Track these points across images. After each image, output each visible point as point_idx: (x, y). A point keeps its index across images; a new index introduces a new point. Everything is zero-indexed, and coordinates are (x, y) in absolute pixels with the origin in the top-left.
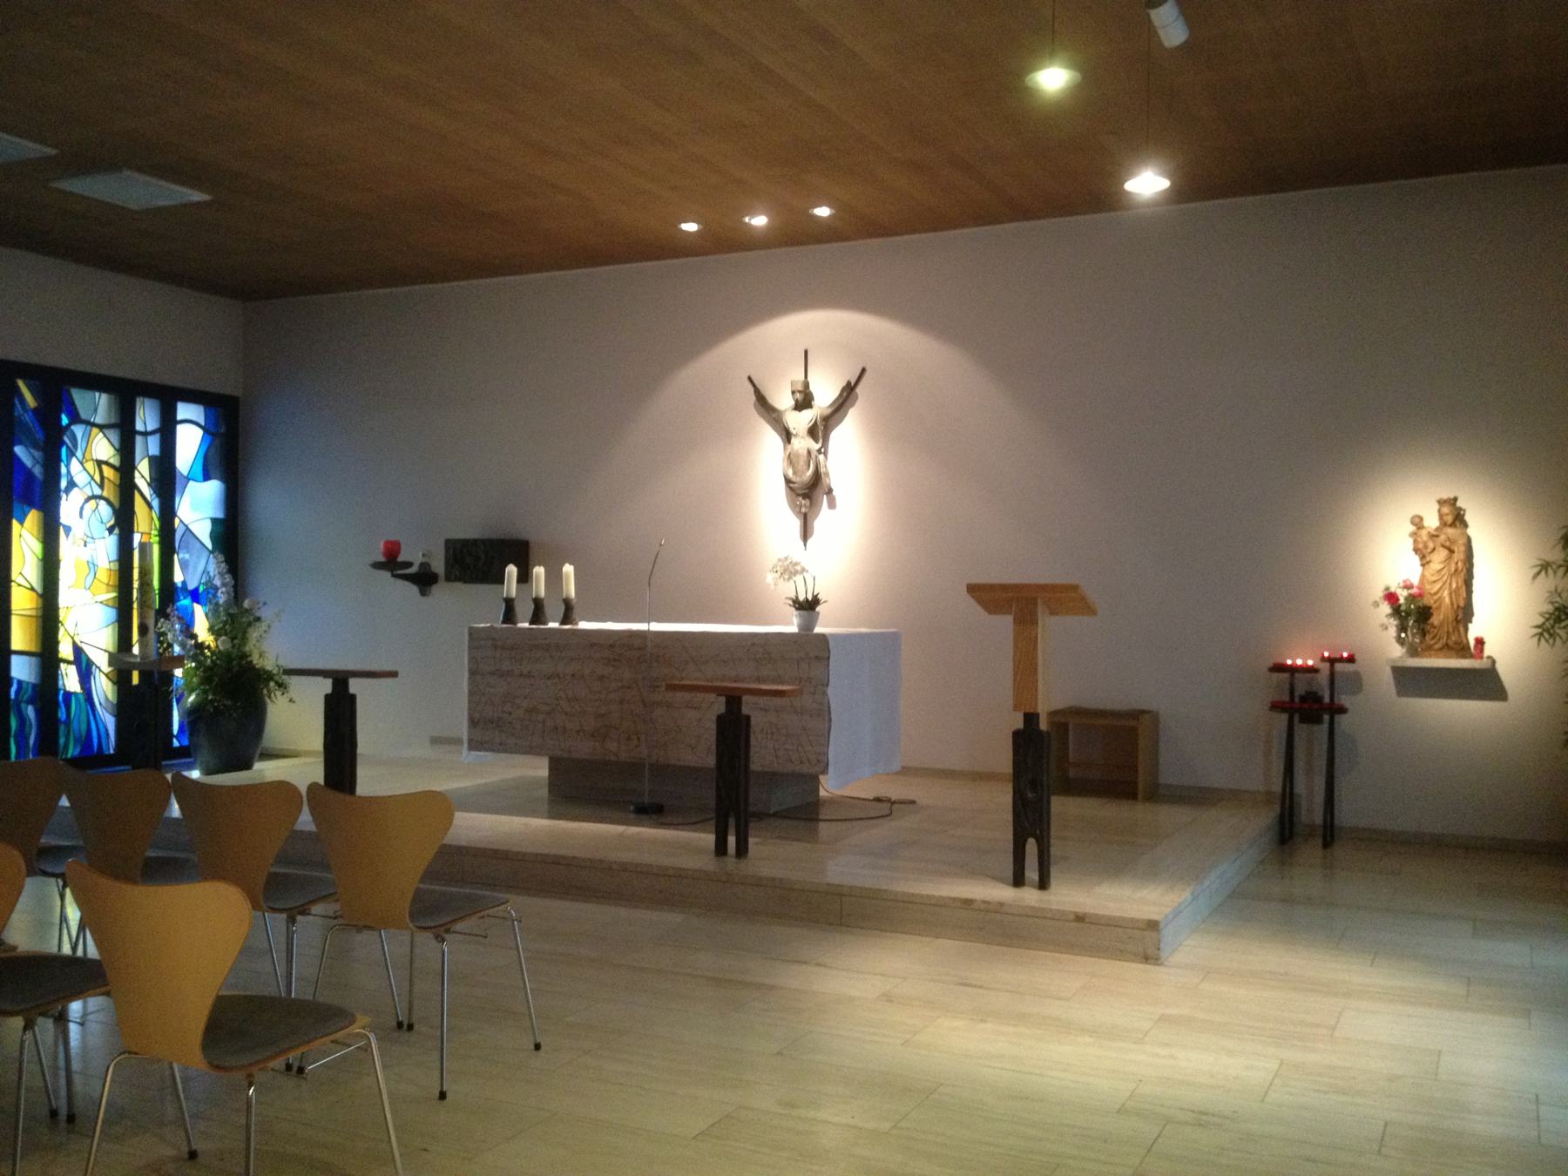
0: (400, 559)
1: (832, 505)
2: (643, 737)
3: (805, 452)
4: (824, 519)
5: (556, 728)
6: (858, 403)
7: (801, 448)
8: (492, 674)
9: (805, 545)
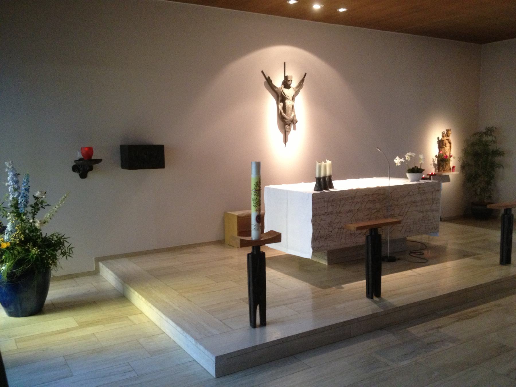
1: (295, 129)
3: (292, 107)
4: (292, 134)
5: (351, 234)
6: (304, 87)
7: (290, 104)
8: (324, 215)
9: (286, 145)
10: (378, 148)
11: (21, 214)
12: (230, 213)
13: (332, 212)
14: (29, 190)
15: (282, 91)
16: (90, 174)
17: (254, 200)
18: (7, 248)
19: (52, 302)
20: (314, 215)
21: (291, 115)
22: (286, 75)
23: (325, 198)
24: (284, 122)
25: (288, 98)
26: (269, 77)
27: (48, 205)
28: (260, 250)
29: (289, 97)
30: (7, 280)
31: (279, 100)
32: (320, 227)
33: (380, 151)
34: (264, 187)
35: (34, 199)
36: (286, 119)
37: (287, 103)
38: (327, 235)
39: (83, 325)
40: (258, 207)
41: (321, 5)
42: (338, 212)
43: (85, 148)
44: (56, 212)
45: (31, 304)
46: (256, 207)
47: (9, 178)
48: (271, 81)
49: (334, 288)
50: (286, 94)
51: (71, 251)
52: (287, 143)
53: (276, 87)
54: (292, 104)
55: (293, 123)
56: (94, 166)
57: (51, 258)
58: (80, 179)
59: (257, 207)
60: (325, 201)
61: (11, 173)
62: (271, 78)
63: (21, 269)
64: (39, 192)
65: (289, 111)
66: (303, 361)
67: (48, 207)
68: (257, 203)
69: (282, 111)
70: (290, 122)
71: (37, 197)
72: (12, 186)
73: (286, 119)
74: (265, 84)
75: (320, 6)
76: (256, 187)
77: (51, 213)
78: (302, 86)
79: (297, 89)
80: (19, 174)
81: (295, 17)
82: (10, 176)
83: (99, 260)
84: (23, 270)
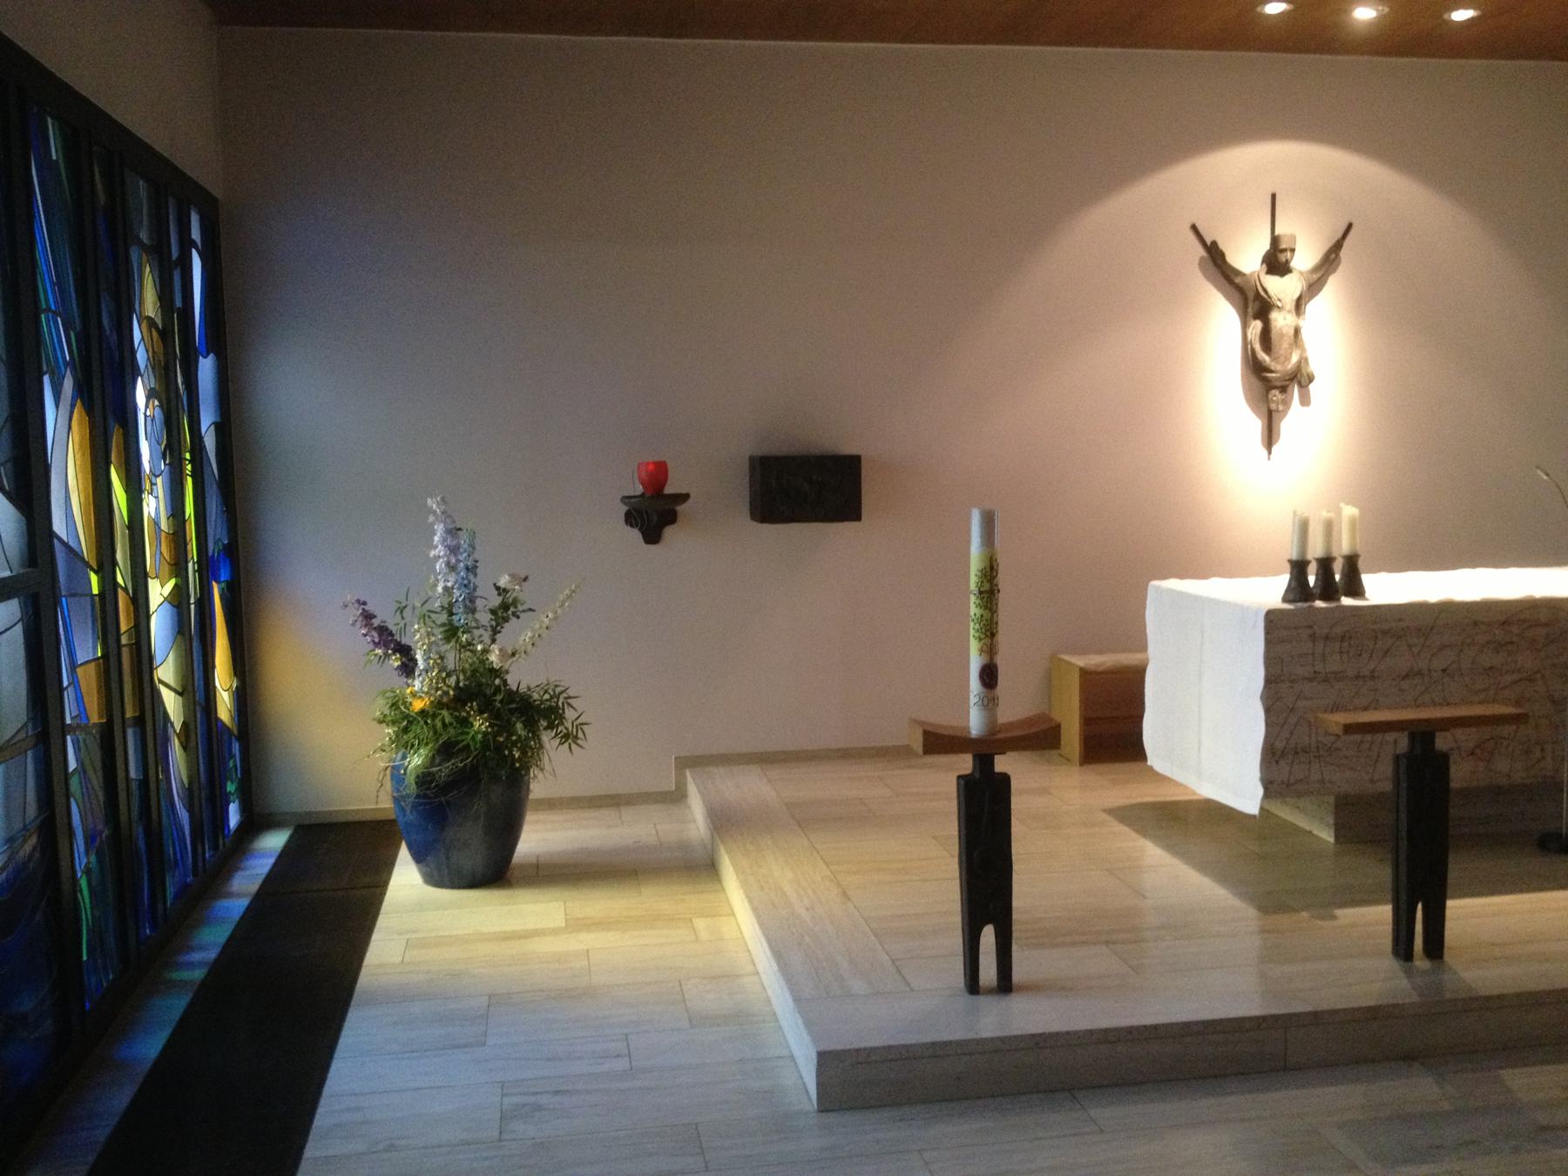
0: (668, 490)
1: (1305, 401)
2: (1548, 747)
3: (1292, 332)
4: (1294, 419)
6: (1341, 268)
7: (1287, 325)
9: (1270, 453)
10: (1537, 467)
11: (458, 628)
13: (1341, 672)
14: (478, 571)
15: (1258, 284)
16: (669, 532)
17: (975, 621)
18: (422, 712)
19: (538, 860)
20: (1271, 681)
21: (1288, 359)
22: (1277, 233)
23: (1315, 627)
24: (1265, 380)
25: (1280, 304)
26: (1214, 244)
27: (530, 610)
28: (994, 769)
29: (1283, 301)
30: (415, 789)
31: (1250, 310)
32: (1293, 719)
33: (1545, 477)
34: (1147, 585)
35: (496, 592)
36: (1271, 372)
37: (1275, 321)
38: (1320, 745)
39: (576, 925)
40: (988, 641)
41: (1380, 8)
42: (1367, 673)
43: (648, 464)
44: (547, 628)
45: (472, 857)
46: (980, 640)
47: (436, 538)
48: (1222, 255)
49: (1305, 914)
50: (1271, 293)
51: (580, 732)
52: (1274, 449)
53: (1238, 273)
54: (1294, 324)
55: (1300, 385)
56: (680, 508)
57: (519, 745)
58: (645, 545)
59: (983, 641)
60: (1313, 637)
61: (442, 526)
62: (1222, 246)
63: (449, 766)
64: (507, 577)
65: (1282, 346)
66: (1092, 1112)
67: (531, 613)
68: (983, 630)
69: (1258, 347)
70: (1286, 380)
71: (504, 590)
72: (443, 557)
73: (1271, 372)
75: (1377, 10)
76: (982, 582)
77: (533, 630)
78: (1334, 264)
79: (1315, 277)
80: (460, 529)
81: (1287, 50)
82: (439, 534)
83: (688, 763)
84: (452, 769)
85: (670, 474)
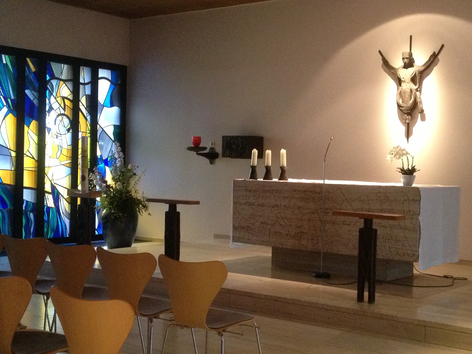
1: (423, 119)
3: (409, 91)
9: (408, 140)
12: (12, 71)
25: (403, 80)
52: (410, 139)
70: (408, 110)
74: (382, 66)
85: (202, 141)
